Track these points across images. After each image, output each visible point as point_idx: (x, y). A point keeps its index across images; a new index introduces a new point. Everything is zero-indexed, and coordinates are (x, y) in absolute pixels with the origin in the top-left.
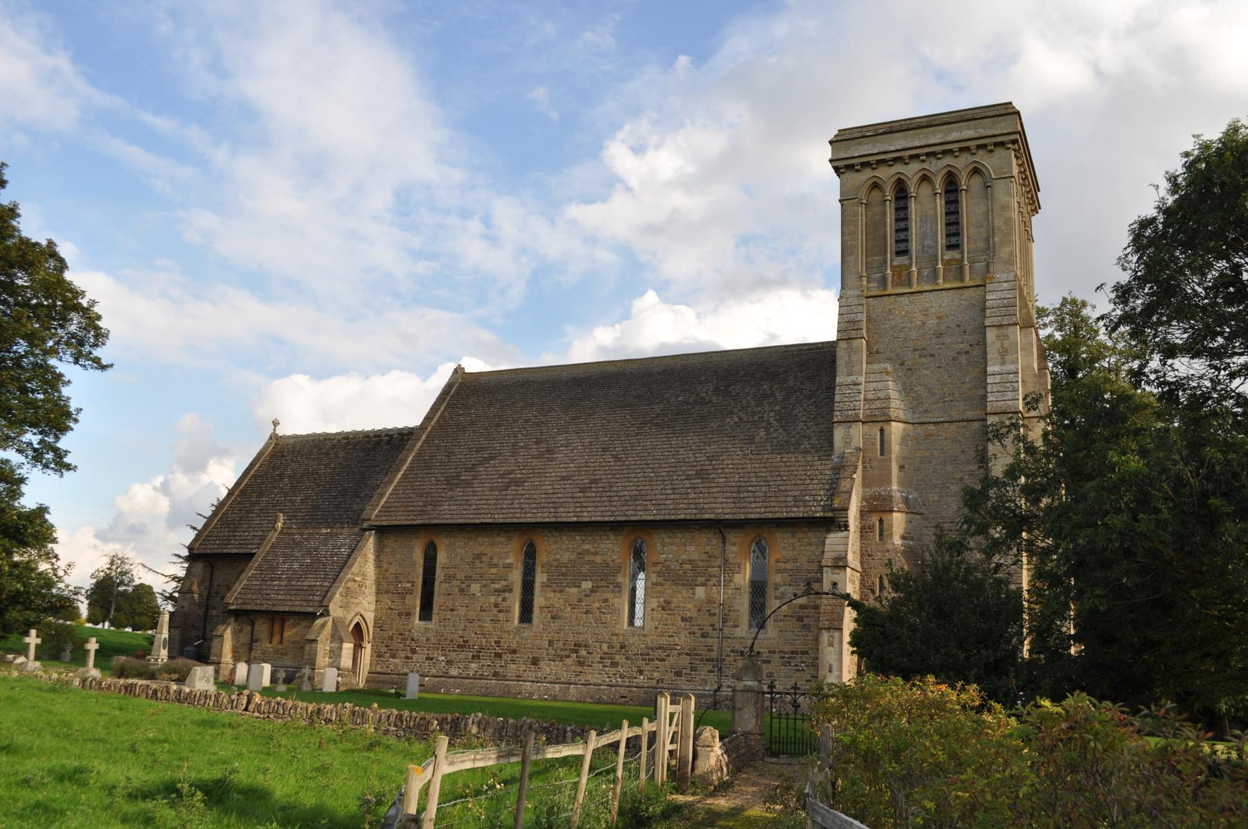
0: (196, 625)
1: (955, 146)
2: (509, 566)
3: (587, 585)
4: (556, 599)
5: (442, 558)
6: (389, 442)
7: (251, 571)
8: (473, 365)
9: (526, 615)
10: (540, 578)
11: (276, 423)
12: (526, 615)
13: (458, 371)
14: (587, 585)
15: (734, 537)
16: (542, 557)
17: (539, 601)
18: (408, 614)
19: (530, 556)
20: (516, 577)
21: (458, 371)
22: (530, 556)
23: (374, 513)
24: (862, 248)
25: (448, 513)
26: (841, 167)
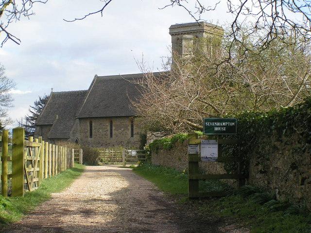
0: (17, 143)
1: (192, 32)
2: (107, 126)
3: (122, 129)
4: (117, 132)
5: (93, 124)
6: (81, 94)
7: (52, 128)
8: (101, 74)
9: (111, 136)
10: (113, 128)
11: (52, 89)
12: (111, 136)
13: (96, 76)
14: (122, 129)
15: (116, 122)
16: (114, 124)
17: (114, 132)
18: (87, 137)
19: (111, 123)
20: (109, 128)
21: (96, 76)
22: (111, 123)
23: (78, 115)
24: (49, 165)
25: (94, 115)
26: (172, 34)
